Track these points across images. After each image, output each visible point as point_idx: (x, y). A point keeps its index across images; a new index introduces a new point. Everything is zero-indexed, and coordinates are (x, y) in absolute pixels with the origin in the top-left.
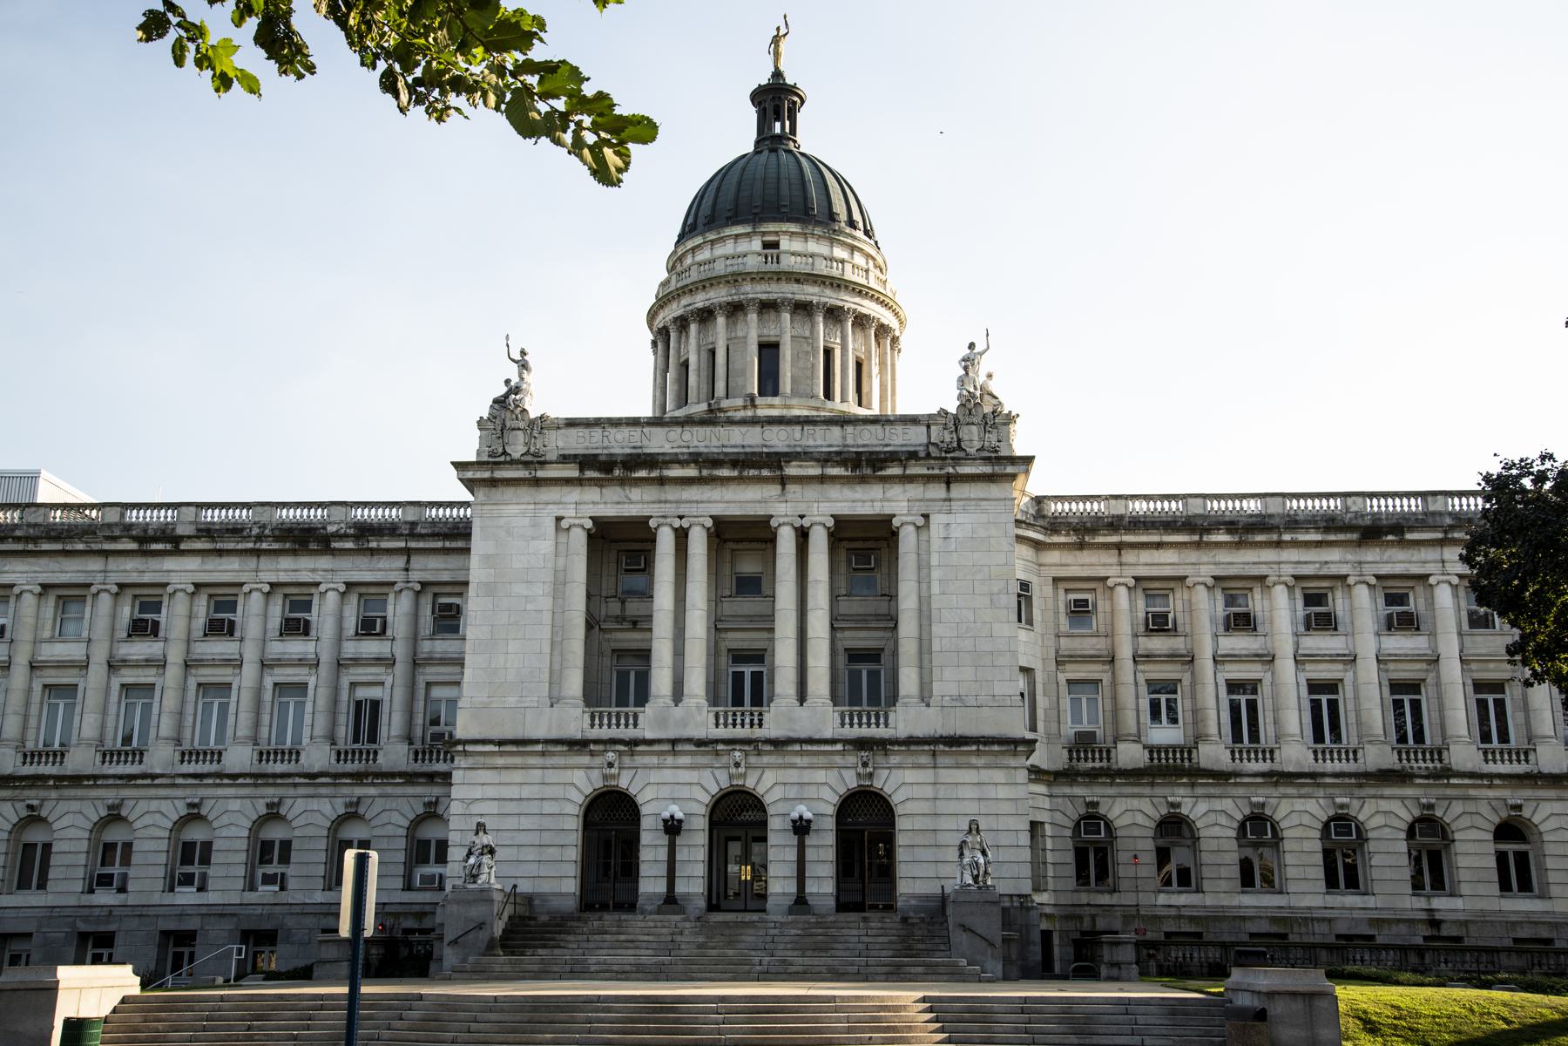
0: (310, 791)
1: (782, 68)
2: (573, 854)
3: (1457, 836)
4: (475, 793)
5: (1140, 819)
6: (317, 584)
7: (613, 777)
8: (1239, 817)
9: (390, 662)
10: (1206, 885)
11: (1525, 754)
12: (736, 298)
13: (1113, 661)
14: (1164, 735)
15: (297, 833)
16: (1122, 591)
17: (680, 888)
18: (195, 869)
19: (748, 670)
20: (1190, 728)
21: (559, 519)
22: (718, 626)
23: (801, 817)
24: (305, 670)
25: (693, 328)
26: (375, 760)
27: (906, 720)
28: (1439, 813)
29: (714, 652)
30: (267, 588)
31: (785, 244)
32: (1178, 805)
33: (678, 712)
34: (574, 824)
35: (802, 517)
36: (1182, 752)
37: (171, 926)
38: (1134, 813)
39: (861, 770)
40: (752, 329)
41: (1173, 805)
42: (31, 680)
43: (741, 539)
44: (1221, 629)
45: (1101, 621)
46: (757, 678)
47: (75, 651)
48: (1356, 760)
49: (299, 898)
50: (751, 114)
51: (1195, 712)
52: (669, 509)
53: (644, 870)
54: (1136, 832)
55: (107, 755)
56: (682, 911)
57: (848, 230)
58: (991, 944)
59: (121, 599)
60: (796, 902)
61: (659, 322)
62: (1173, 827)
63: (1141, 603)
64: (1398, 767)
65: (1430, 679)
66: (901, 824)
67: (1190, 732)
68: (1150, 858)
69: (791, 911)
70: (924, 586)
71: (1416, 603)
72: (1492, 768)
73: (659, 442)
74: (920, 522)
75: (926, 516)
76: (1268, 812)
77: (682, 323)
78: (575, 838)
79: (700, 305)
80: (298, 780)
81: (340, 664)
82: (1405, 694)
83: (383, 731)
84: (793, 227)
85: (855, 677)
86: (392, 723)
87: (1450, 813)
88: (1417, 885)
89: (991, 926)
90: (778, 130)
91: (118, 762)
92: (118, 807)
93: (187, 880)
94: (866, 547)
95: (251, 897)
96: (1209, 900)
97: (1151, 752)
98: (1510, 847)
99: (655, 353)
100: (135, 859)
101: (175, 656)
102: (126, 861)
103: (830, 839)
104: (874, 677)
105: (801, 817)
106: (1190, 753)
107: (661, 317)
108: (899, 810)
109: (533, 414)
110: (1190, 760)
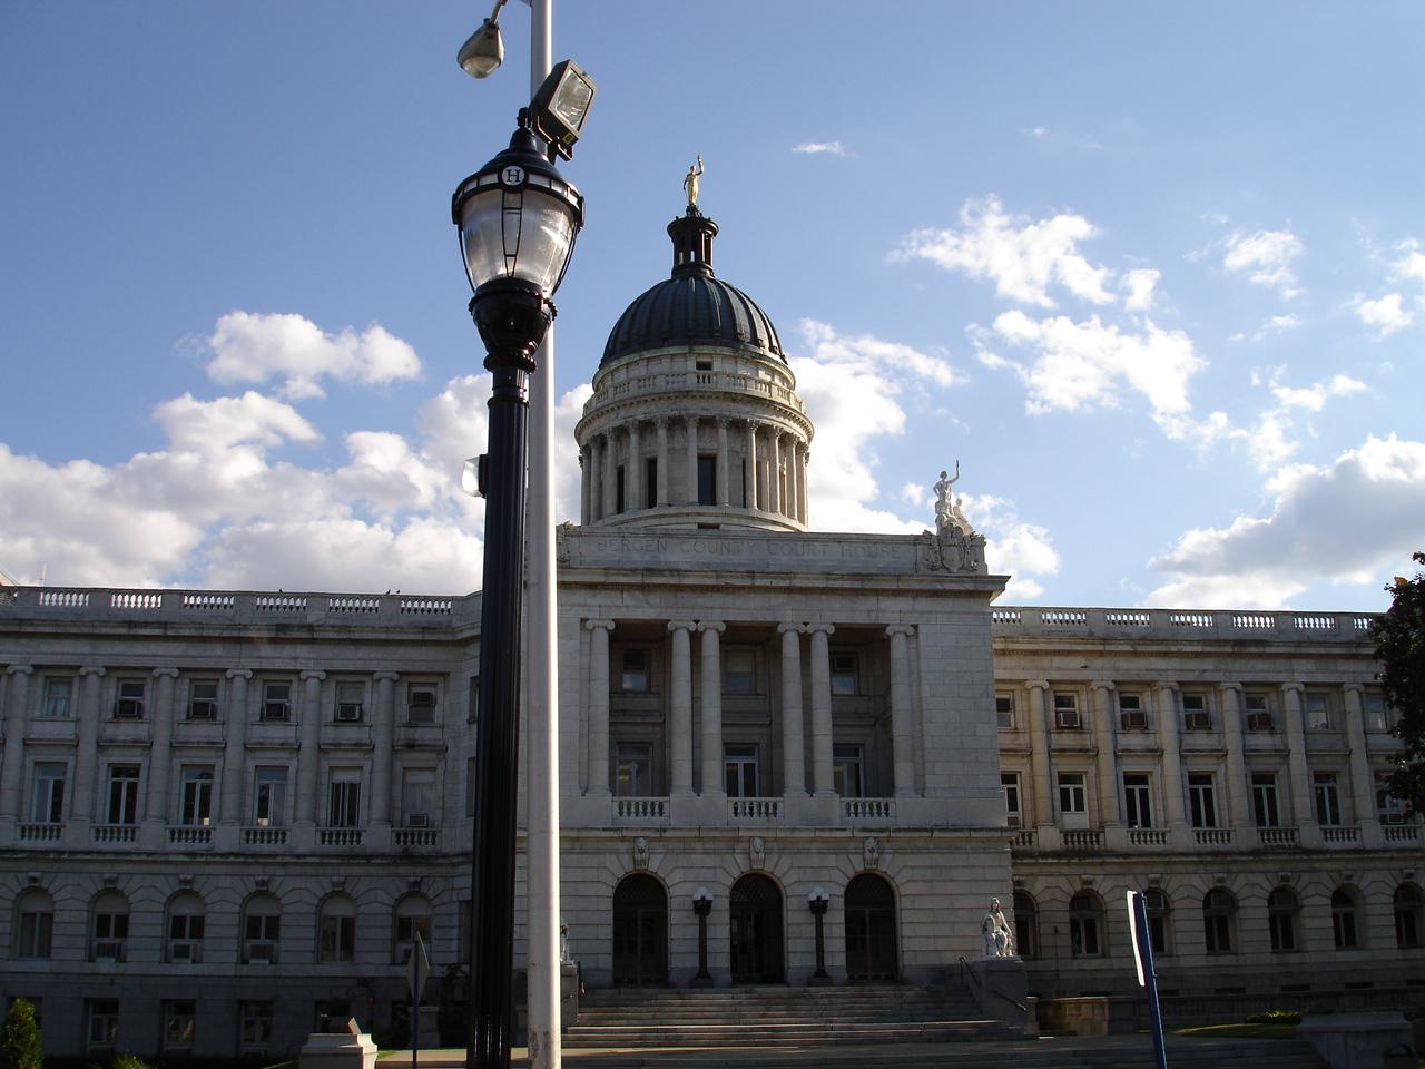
0: (298, 869)
3: (1305, 902)
5: (1059, 895)
9: (369, 748)
11: (1352, 833)
14: (1076, 820)
17: (828, 962)
21: (583, 621)
24: (285, 754)
26: (359, 842)
28: (1292, 884)
30: (249, 675)
31: (717, 366)
34: (608, 905)
35: (806, 624)
36: (1091, 836)
39: (868, 856)
40: (693, 442)
42: (24, 756)
44: (1119, 726)
45: (1019, 719)
47: (64, 730)
50: (668, 246)
53: (674, 947)
55: (26, 831)
57: (771, 355)
60: (698, 976)
64: (1262, 846)
66: (903, 903)
67: (1096, 817)
68: (1065, 929)
71: (1270, 703)
74: (911, 631)
75: (915, 627)
76: (1162, 887)
77: (621, 432)
78: (611, 915)
79: (642, 417)
80: (286, 860)
81: (321, 749)
82: (1262, 782)
83: (363, 814)
84: (727, 351)
86: (372, 809)
87: (1302, 884)
91: (37, 837)
92: (113, 881)
93: (182, 952)
95: (245, 970)
97: (1066, 836)
98: (1342, 910)
100: (132, 931)
101: (162, 739)
105: (703, 898)
106: (1097, 836)
110: (1098, 841)
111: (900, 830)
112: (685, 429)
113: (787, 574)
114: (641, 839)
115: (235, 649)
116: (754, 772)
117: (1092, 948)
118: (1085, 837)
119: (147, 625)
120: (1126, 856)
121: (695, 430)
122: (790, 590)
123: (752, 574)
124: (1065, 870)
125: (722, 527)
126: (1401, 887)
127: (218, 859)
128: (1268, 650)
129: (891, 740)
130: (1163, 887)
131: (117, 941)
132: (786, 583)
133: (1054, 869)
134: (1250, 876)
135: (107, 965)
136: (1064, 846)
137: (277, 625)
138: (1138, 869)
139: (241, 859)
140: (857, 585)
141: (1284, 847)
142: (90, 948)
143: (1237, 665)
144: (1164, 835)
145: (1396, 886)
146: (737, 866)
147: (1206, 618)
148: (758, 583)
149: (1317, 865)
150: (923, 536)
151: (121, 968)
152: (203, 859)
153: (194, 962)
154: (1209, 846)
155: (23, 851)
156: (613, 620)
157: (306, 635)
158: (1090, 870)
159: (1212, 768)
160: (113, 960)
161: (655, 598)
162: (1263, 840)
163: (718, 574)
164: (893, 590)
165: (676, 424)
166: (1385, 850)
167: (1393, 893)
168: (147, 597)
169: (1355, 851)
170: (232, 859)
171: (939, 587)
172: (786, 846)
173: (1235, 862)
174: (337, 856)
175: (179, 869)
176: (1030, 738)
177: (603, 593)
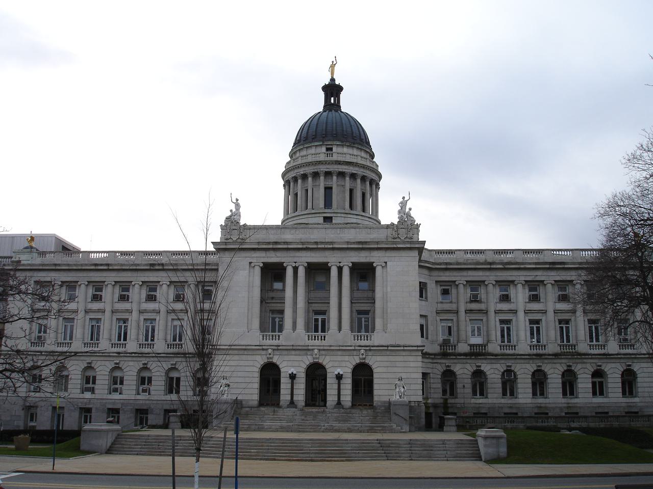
1: (334, 77)
2: (257, 386)
3: (549, 377)
4: (221, 366)
5: (466, 371)
6: (159, 282)
7: (271, 358)
8: (502, 371)
10: (489, 396)
12: (316, 170)
13: (457, 312)
15: (153, 374)
16: (461, 286)
17: (295, 398)
18: (118, 386)
19: (320, 317)
20: (485, 337)
21: (250, 263)
22: (309, 302)
23: (339, 373)
24: (155, 314)
25: (300, 181)
27: (378, 338)
29: (307, 311)
30: (141, 283)
31: (335, 149)
32: (480, 366)
33: (294, 335)
34: (257, 375)
35: (340, 263)
37: (110, 407)
38: (463, 370)
39: (361, 356)
40: (348, 182)
41: (477, 366)
43: (318, 272)
46: (323, 321)
48: (545, 349)
49: (155, 398)
50: (322, 95)
51: (488, 331)
52: (290, 259)
53: (282, 392)
54: (464, 376)
56: (296, 407)
58: (405, 420)
59: (89, 287)
60: (337, 404)
61: (286, 178)
62: (478, 375)
63: (469, 291)
64: (559, 352)
65: (573, 319)
69: (335, 407)
70: (385, 288)
72: (592, 352)
73: (288, 236)
75: (386, 263)
76: (512, 369)
77: (295, 179)
78: (257, 380)
79: (302, 173)
85: (360, 320)
87: (577, 368)
88: (564, 394)
89: (405, 413)
90: (332, 101)
93: (116, 390)
94: (364, 273)
95: (139, 397)
96: (490, 401)
98: (597, 380)
99: (285, 189)
100: (97, 382)
101: (108, 309)
102: (94, 383)
103: (350, 381)
104: (367, 321)
105: (339, 373)
106: (485, 347)
107: (287, 176)
108: (375, 371)
109: (242, 223)
110: (485, 349)
111: (374, 346)
112: (332, 176)
113: (332, 243)
114: (270, 350)
115: (135, 274)
116: (318, 325)
117: (542, 394)
118: (566, 347)
119: (101, 265)
120: (496, 355)
121: (323, 177)
122: (333, 249)
123: (316, 243)
124: (469, 361)
125: (321, 220)
126: (625, 371)
127: (128, 355)
128: (566, 266)
129: (260, 317)
130: (603, 368)
131: (93, 386)
132: (331, 246)
133: (464, 361)
134: (554, 365)
135: (88, 395)
136: (470, 351)
137: (150, 264)
138: (503, 361)
139: (137, 355)
140: (360, 246)
141: (570, 352)
142: (83, 388)
143: (553, 273)
144: (515, 346)
145: (622, 370)
146: (308, 360)
147: (586, 252)
148: (319, 246)
149: (585, 361)
150: (391, 224)
151: (93, 396)
152: (123, 355)
153: (120, 394)
154: (535, 352)
155: (57, 352)
156: (262, 262)
157: (161, 268)
158: (480, 361)
159: (540, 318)
160: (90, 393)
161: (279, 254)
162: (561, 349)
163: (303, 243)
164: (376, 248)
165: (316, 175)
166: (617, 354)
167: (621, 373)
168: (100, 254)
169: (604, 354)
170: (133, 355)
171: (395, 246)
172: (329, 350)
173: (546, 359)
174: (172, 354)
175: (114, 359)
176: (487, 305)
177: (258, 252)
